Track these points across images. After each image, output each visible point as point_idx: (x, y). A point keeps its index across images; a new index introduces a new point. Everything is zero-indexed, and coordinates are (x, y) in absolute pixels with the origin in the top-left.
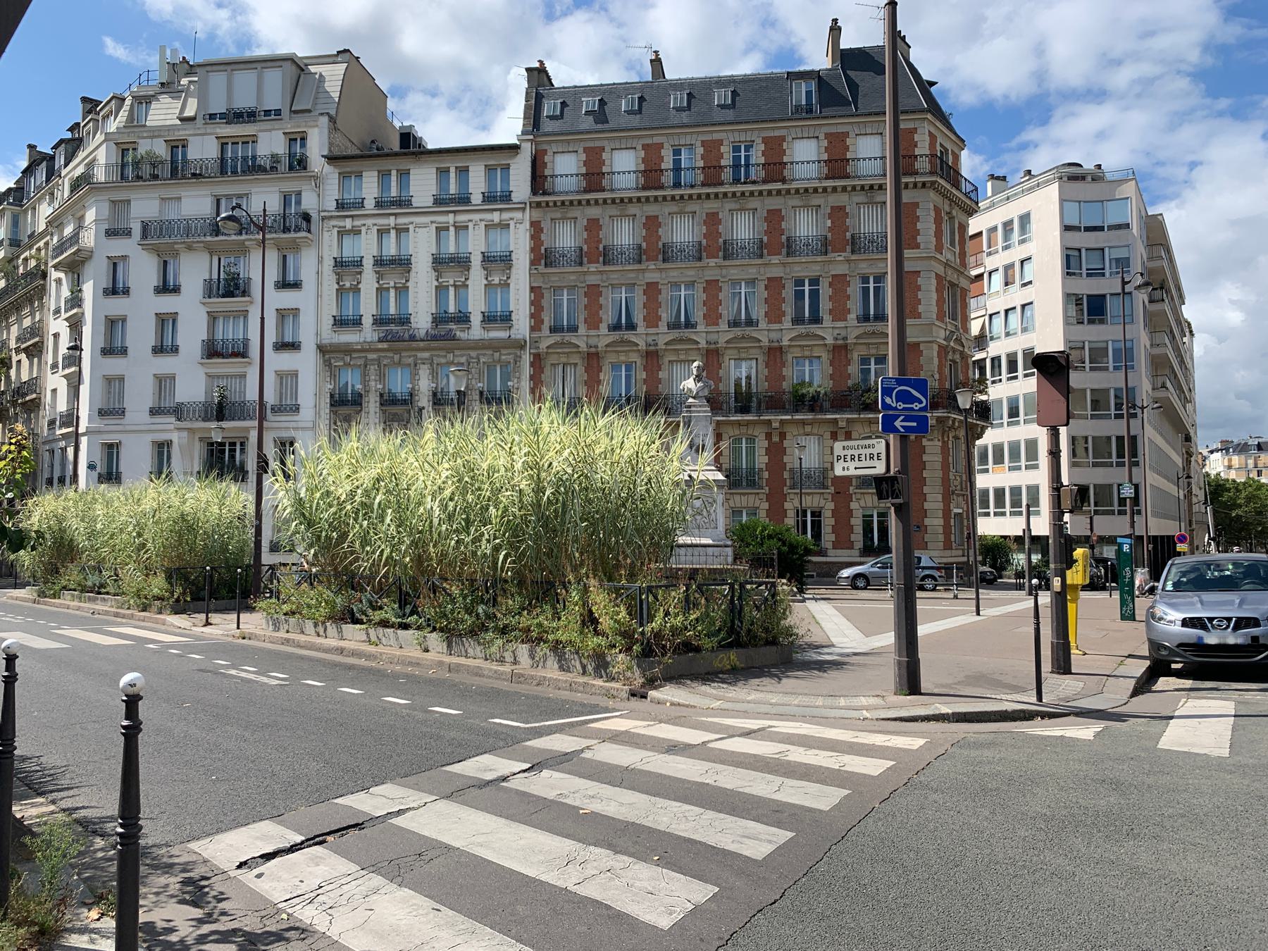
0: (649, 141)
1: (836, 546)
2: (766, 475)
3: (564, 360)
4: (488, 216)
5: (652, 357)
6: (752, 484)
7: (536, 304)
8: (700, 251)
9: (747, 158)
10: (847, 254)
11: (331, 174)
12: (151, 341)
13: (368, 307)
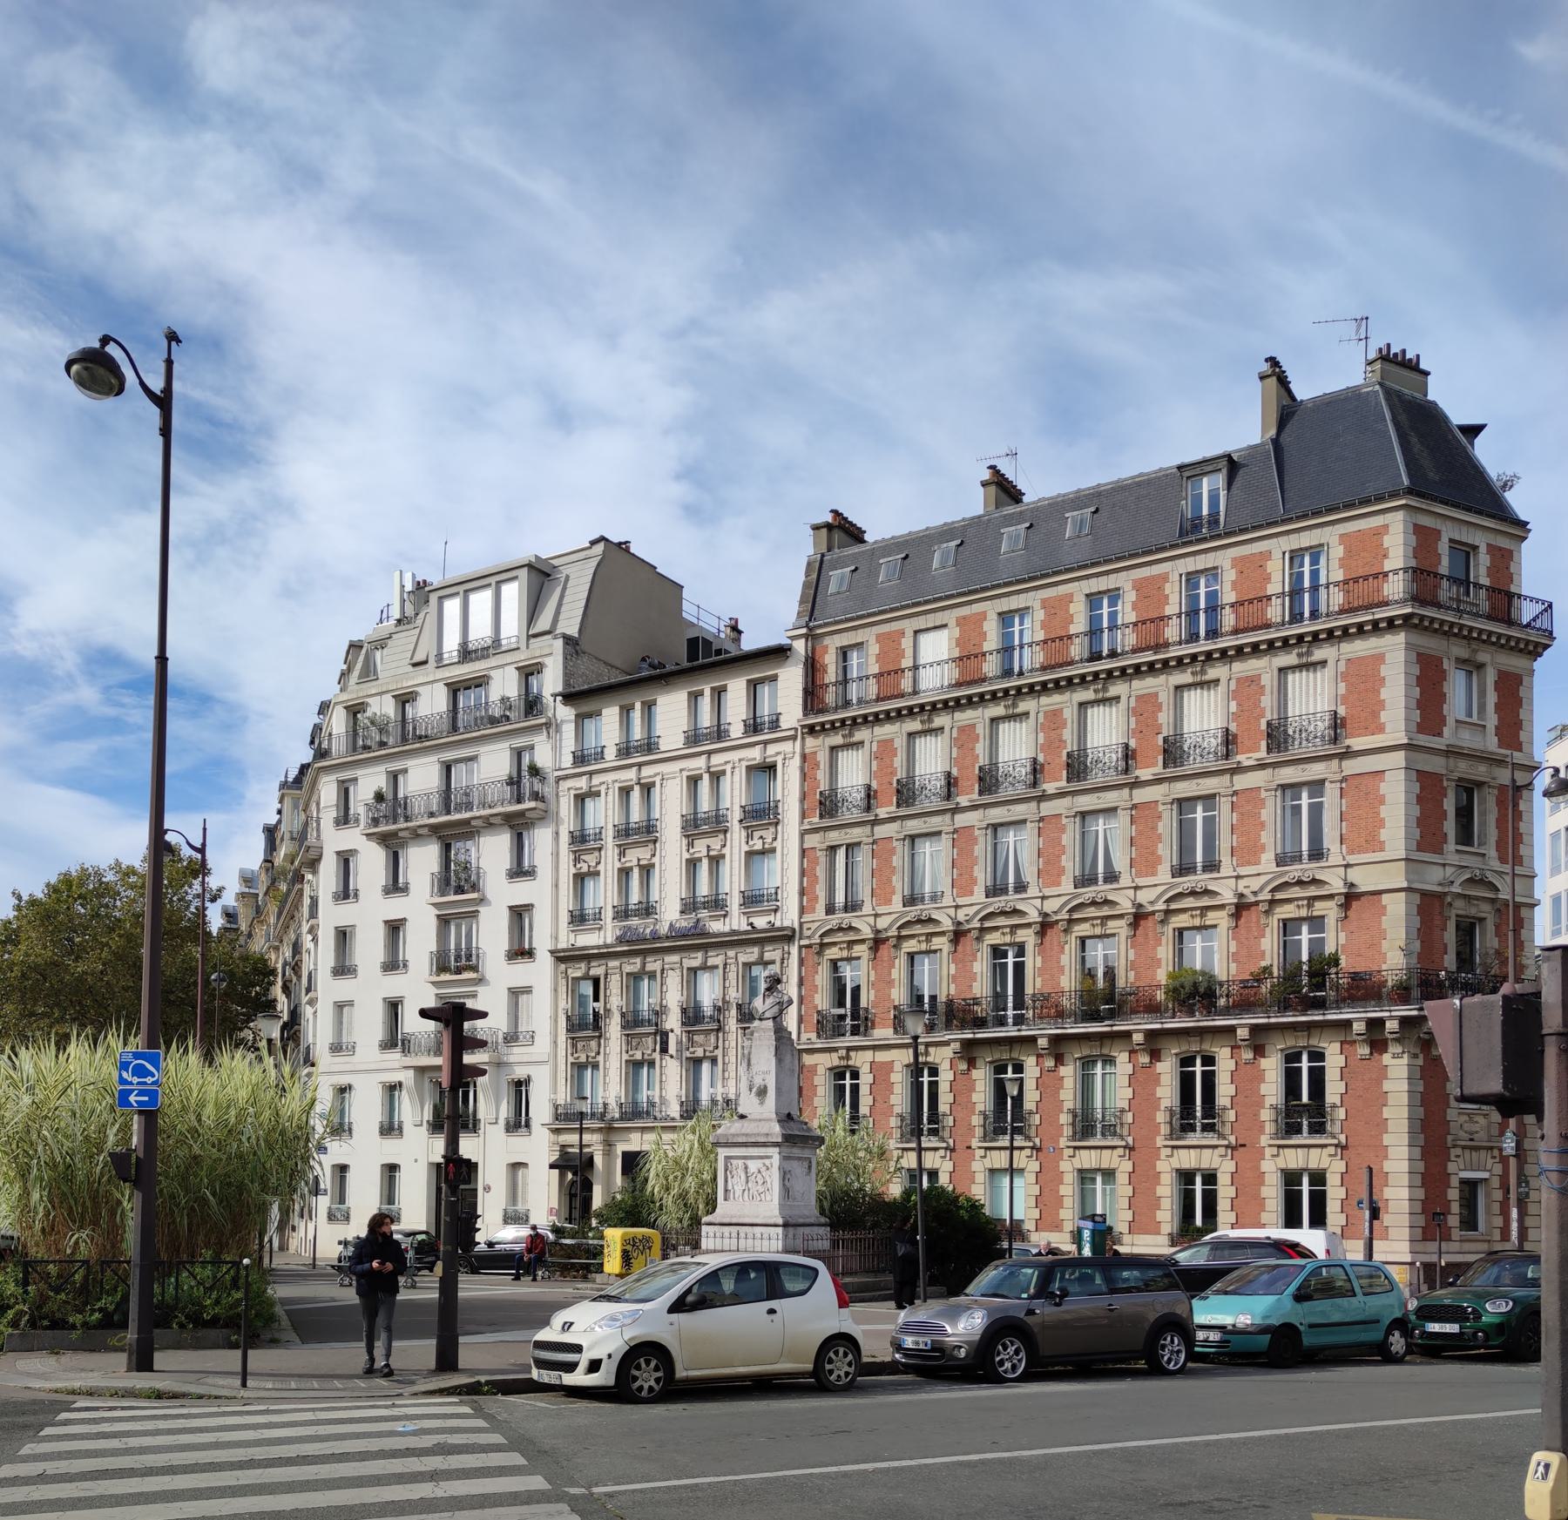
9: (1315, 574)
11: (565, 713)
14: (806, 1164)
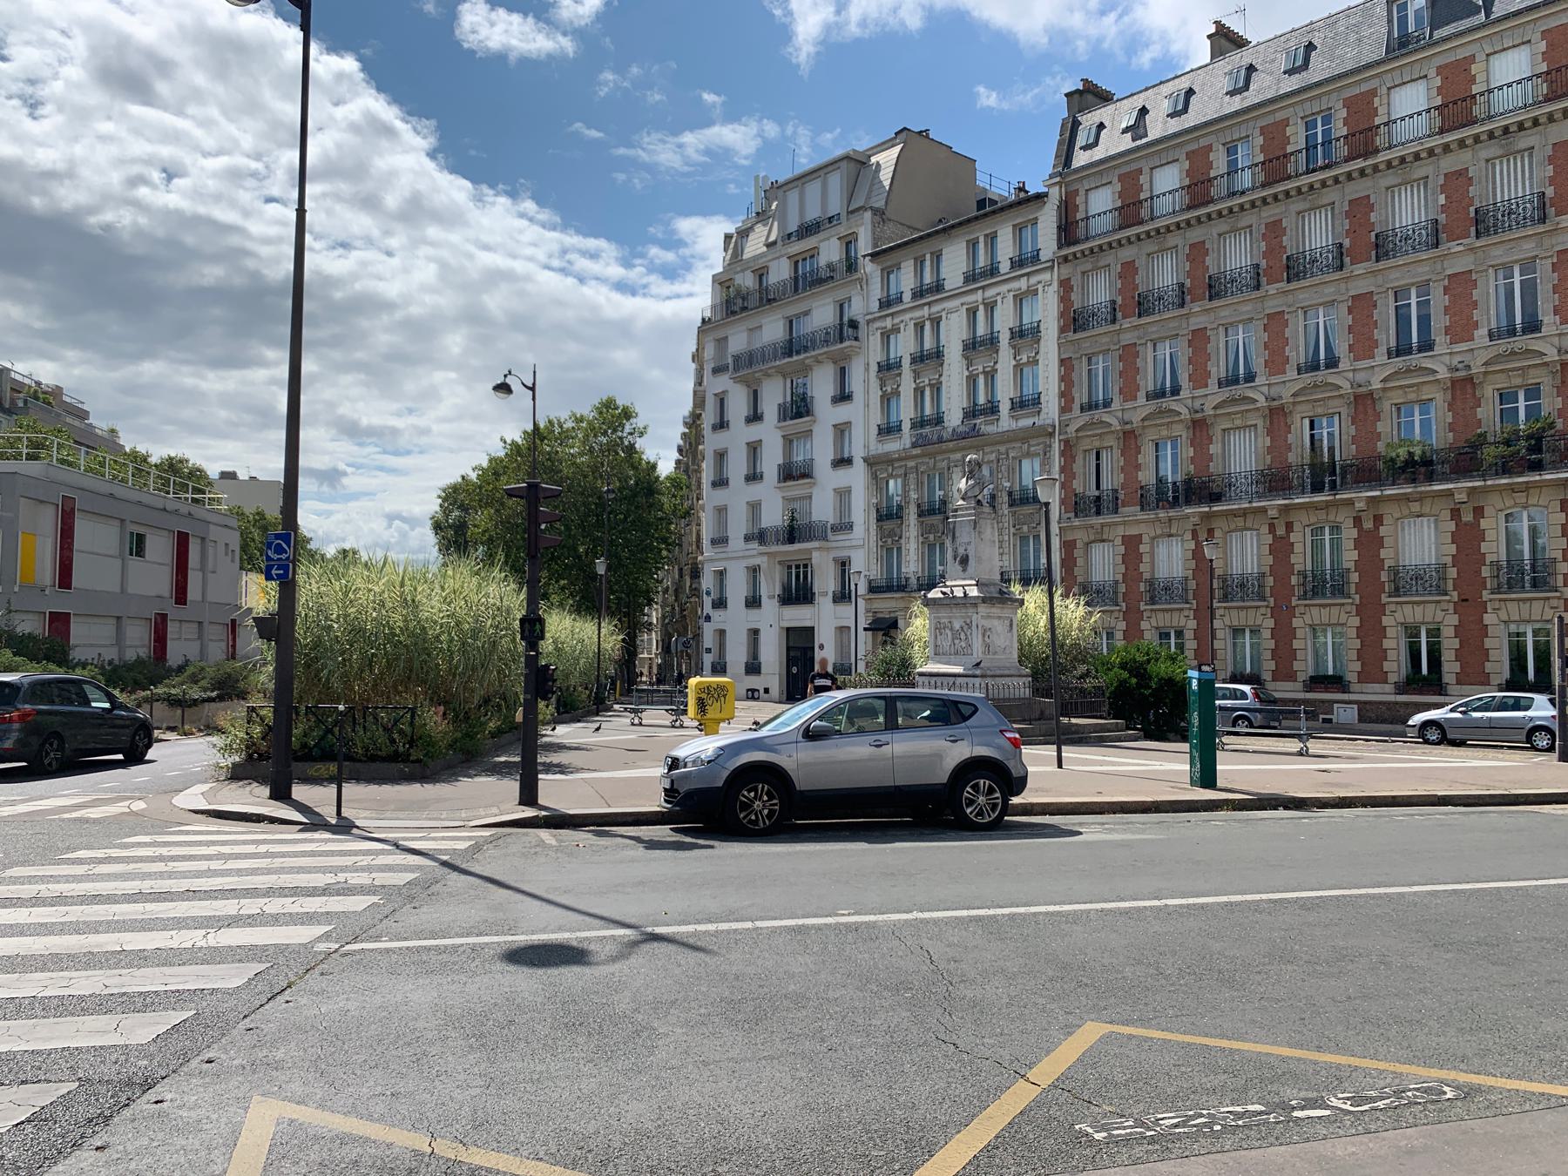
0: (1194, 146)
1: (1364, 677)
2: (1355, 577)
3: (1097, 444)
4: (1014, 285)
5: (1199, 426)
6: (1340, 590)
7: (1066, 379)
8: (1543, 206)
10: (1471, 240)
12: (744, 471)
13: (906, 411)
14: (1007, 623)
